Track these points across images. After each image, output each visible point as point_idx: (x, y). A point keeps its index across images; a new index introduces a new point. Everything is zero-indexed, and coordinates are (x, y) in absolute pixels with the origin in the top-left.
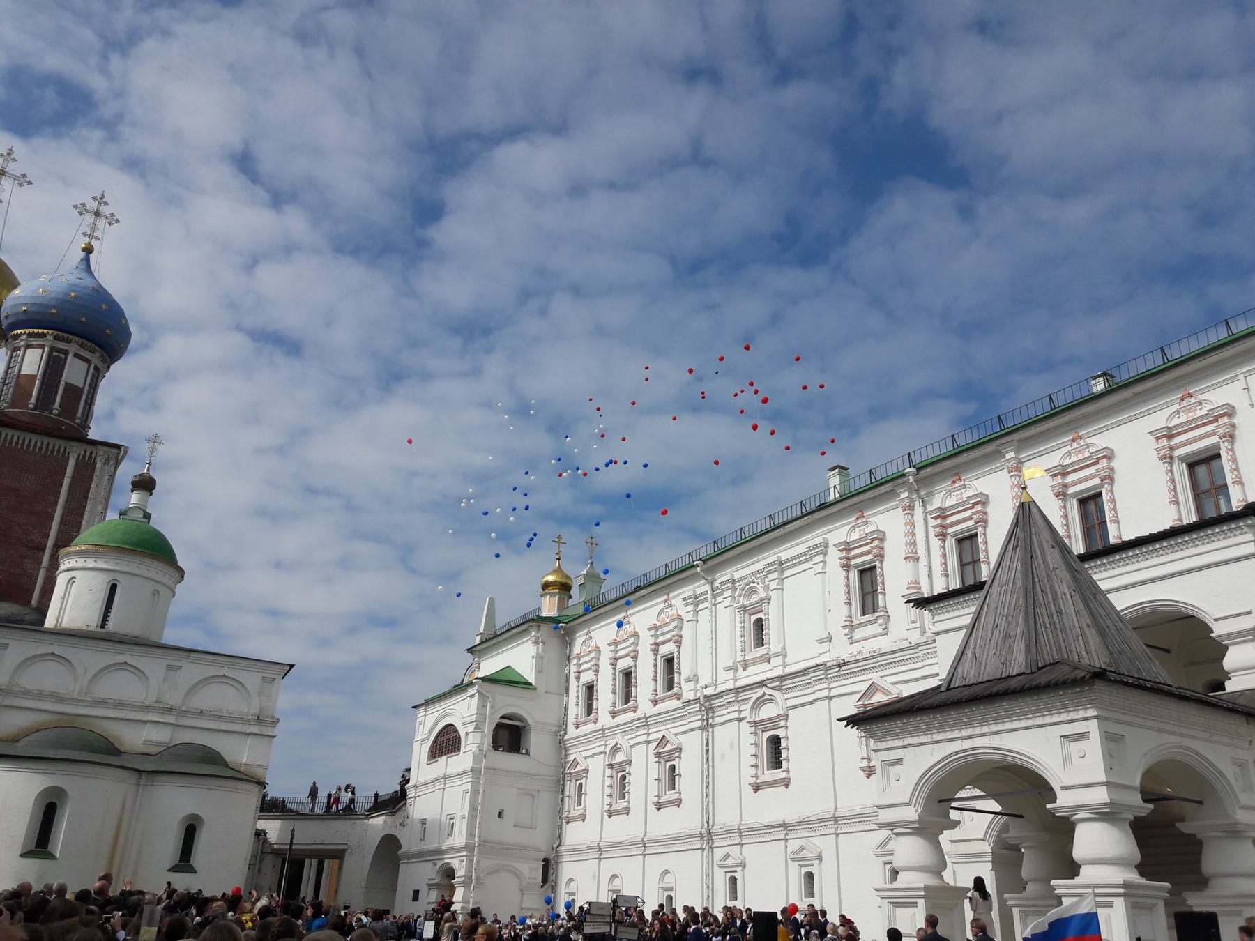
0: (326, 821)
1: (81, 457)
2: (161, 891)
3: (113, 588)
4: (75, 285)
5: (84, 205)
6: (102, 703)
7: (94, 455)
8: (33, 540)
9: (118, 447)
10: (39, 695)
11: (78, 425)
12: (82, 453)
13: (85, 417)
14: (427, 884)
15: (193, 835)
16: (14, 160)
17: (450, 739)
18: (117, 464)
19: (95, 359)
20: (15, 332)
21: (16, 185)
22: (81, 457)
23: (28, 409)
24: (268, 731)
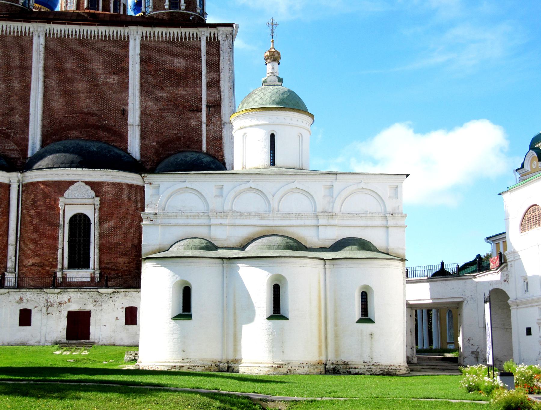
0: (443, 282)
1: (208, 39)
3: (273, 136)
6: (288, 215)
7: (216, 35)
8: (193, 105)
9: (231, 25)
11: (199, 14)
12: (209, 35)
13: (202, 6)
14: (537, 323)
15: (366, 298)
17: (530, 217)
18: (233, 38)
22: (208, 39)
23: (165, 9)
24: (401, 223)
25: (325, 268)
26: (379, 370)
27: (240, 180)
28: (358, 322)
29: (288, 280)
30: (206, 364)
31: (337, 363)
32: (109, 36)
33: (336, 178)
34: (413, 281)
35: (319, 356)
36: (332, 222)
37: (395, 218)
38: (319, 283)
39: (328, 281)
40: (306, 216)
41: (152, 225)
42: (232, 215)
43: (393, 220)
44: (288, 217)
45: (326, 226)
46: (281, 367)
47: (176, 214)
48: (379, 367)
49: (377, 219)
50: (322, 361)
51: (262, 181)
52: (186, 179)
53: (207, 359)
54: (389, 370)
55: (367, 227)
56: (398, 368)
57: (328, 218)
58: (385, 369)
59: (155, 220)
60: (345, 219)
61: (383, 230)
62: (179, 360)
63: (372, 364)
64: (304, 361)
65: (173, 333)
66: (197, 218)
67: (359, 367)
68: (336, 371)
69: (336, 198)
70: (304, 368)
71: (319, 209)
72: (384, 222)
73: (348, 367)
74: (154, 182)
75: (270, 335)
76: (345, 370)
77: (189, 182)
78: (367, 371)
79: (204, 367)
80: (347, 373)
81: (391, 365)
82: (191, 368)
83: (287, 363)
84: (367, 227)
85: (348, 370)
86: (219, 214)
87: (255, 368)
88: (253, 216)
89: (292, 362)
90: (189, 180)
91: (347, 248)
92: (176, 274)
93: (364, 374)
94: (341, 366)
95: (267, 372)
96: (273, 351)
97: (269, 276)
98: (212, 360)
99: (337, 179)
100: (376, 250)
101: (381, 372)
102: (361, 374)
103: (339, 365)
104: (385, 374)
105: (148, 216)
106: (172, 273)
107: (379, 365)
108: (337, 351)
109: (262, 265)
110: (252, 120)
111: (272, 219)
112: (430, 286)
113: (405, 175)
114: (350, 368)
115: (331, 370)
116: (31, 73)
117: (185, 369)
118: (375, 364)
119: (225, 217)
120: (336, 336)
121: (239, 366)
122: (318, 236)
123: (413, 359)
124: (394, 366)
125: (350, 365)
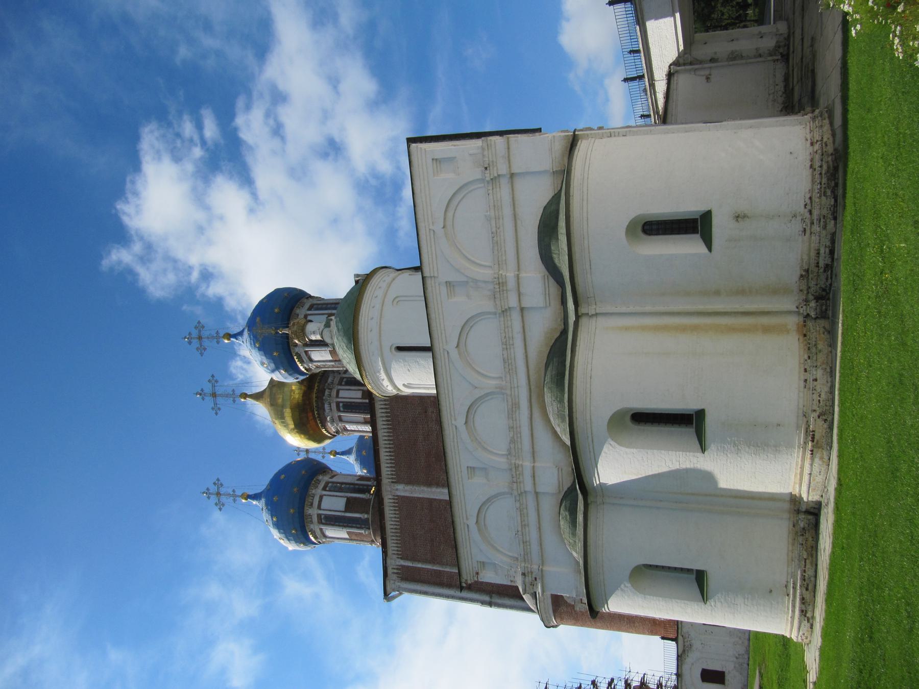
2: (819, 497)
3: (400, 349)
4: (251, 344)
5: (198, 349)
6: (508, 364)
10: (513, 428)
16: (202, 390)
19: (301, 312)
20: (305, 371)
21: (218, 384)
25: (596, 315)
26: (823, 198)
27: (456, 440)
28: (709, 244)
29: (621, 407)
30: (800, 556)
31: (805, 292)
32: (387, 416)
33: (431, 277)
34: (645, 48)
35: (788, 331)
36: (511, 284)
37: (493, 161)
38: (627, 329)
39: (624, 309)
40: (506, 330)
41: (542, 580)
42: (515, 456)
43: (496, 165)
44: (510, 362)
45: (519, 294)
46: (814, 435)
47: (521, 544)
48: (816, 200)
49: (499, 197)
50: (798, 324)
51: (452, 405)
52: (464, 523)
53: (788, 550)
54: (823, 172)
55: (515, 216)
56: (817, 147)
57: (505, 292)
58: (821, 184)
59: (534, 574)
60: (504, 258)
61: (519, 183)
62: (789, 602)
63: (807, 215)
64: (799, 377)
65: (734, 604)
66: (525, 510)
67: (814, 245)
68: (824, 293)
69: (467, 276)
70: (816, 380)
71: (488, 306)
72: (504, 182)
73: (816, 270)
74: (474, 569)
75: (738, 449)
76: (823, 277)
77: (467, 519)
78: (825, 227)
79: (805, 559)
80: (830, 271)
81: (811, 167)
82: (808, 585)
83: (805, 420)
84: (515, 216)
85: (822, 270)
86: (515, 479)
87: (814, 480)
88: (515, 423)
89: (801, 406)
90: (465, 518)
91: (556, 261)
92: (620, 586)
93: (833, 235)
94: (812, 283)
95: (823, 462)
96: (775, 446)
97: (612, 443)
98: (791, 541)
99: (432, 275)
100: (556, 199)
101: (829, 193)
102: (833, 241)
103: (809, 288)
104: (833, 184)
105: (528, 585)
106: (618, 592)
107: (810, 198)
108: (775, 291)
109: (592, 454)
110: (382, 378)
111: (516, 389)
112: (650, 19)
113: (409, 147)
114: (818, 266)
115: (822, 305)
116: (435, 499)
117: (808, 595)
118: (809, 207)
119: (520, 469)
120: (742, 292)
121: (805, 499)
122: (541, 308)
123: (781, 34)
124: (812, 160)
125: (809, 266)
